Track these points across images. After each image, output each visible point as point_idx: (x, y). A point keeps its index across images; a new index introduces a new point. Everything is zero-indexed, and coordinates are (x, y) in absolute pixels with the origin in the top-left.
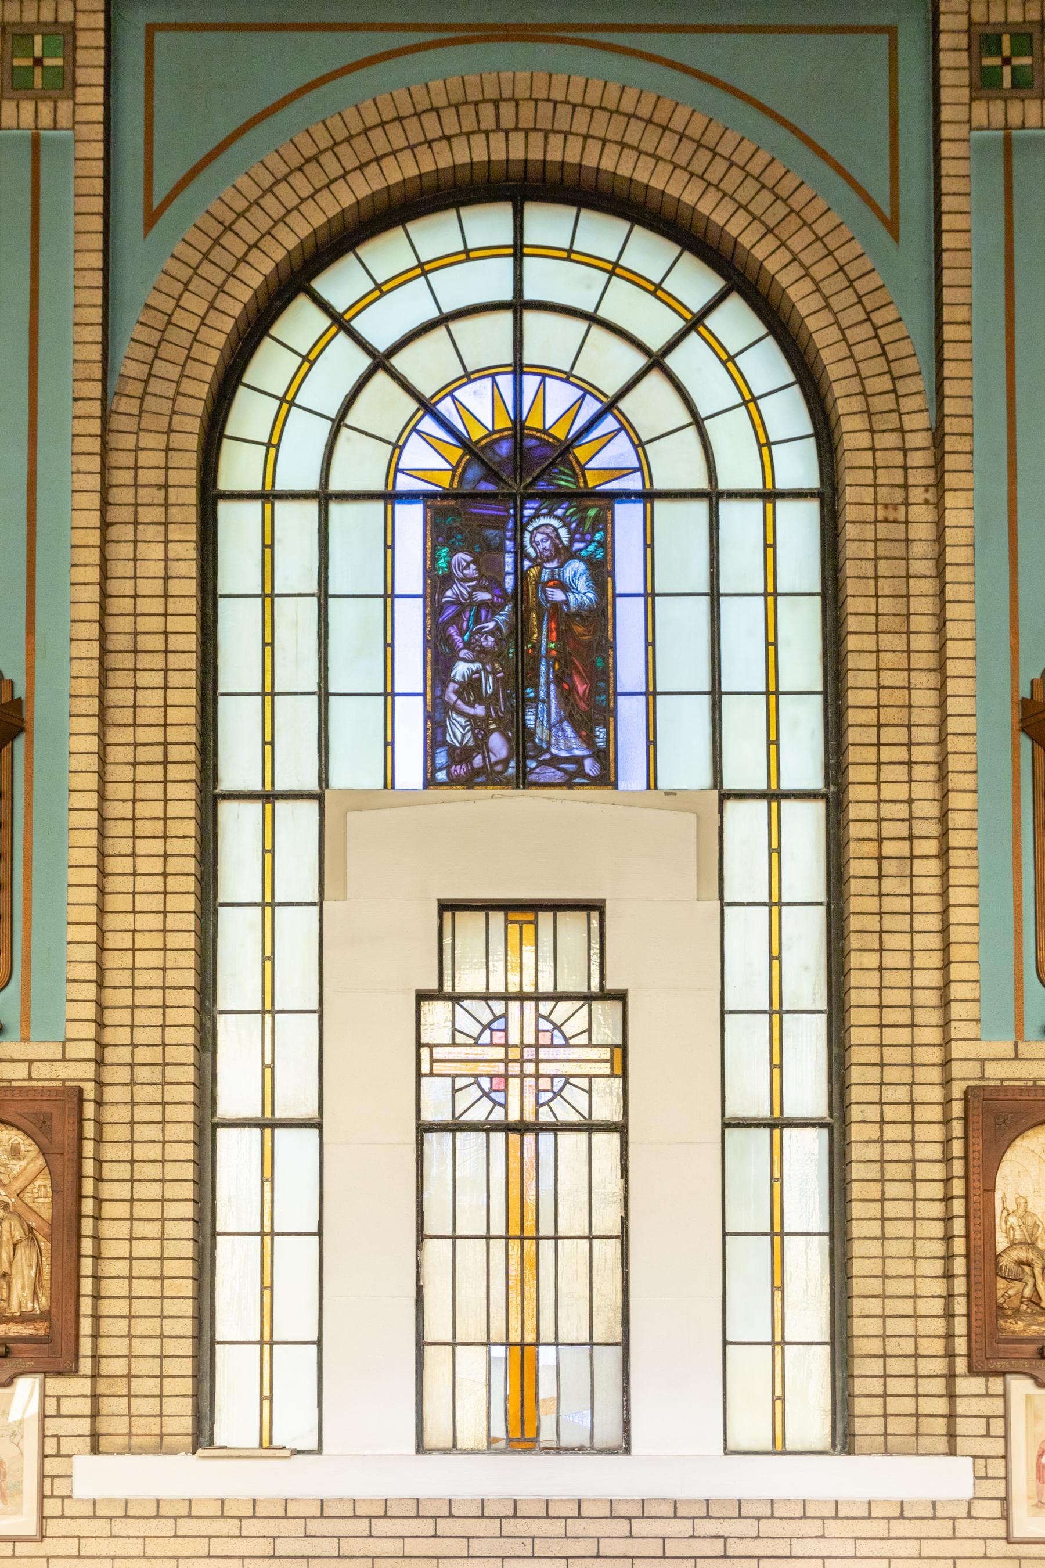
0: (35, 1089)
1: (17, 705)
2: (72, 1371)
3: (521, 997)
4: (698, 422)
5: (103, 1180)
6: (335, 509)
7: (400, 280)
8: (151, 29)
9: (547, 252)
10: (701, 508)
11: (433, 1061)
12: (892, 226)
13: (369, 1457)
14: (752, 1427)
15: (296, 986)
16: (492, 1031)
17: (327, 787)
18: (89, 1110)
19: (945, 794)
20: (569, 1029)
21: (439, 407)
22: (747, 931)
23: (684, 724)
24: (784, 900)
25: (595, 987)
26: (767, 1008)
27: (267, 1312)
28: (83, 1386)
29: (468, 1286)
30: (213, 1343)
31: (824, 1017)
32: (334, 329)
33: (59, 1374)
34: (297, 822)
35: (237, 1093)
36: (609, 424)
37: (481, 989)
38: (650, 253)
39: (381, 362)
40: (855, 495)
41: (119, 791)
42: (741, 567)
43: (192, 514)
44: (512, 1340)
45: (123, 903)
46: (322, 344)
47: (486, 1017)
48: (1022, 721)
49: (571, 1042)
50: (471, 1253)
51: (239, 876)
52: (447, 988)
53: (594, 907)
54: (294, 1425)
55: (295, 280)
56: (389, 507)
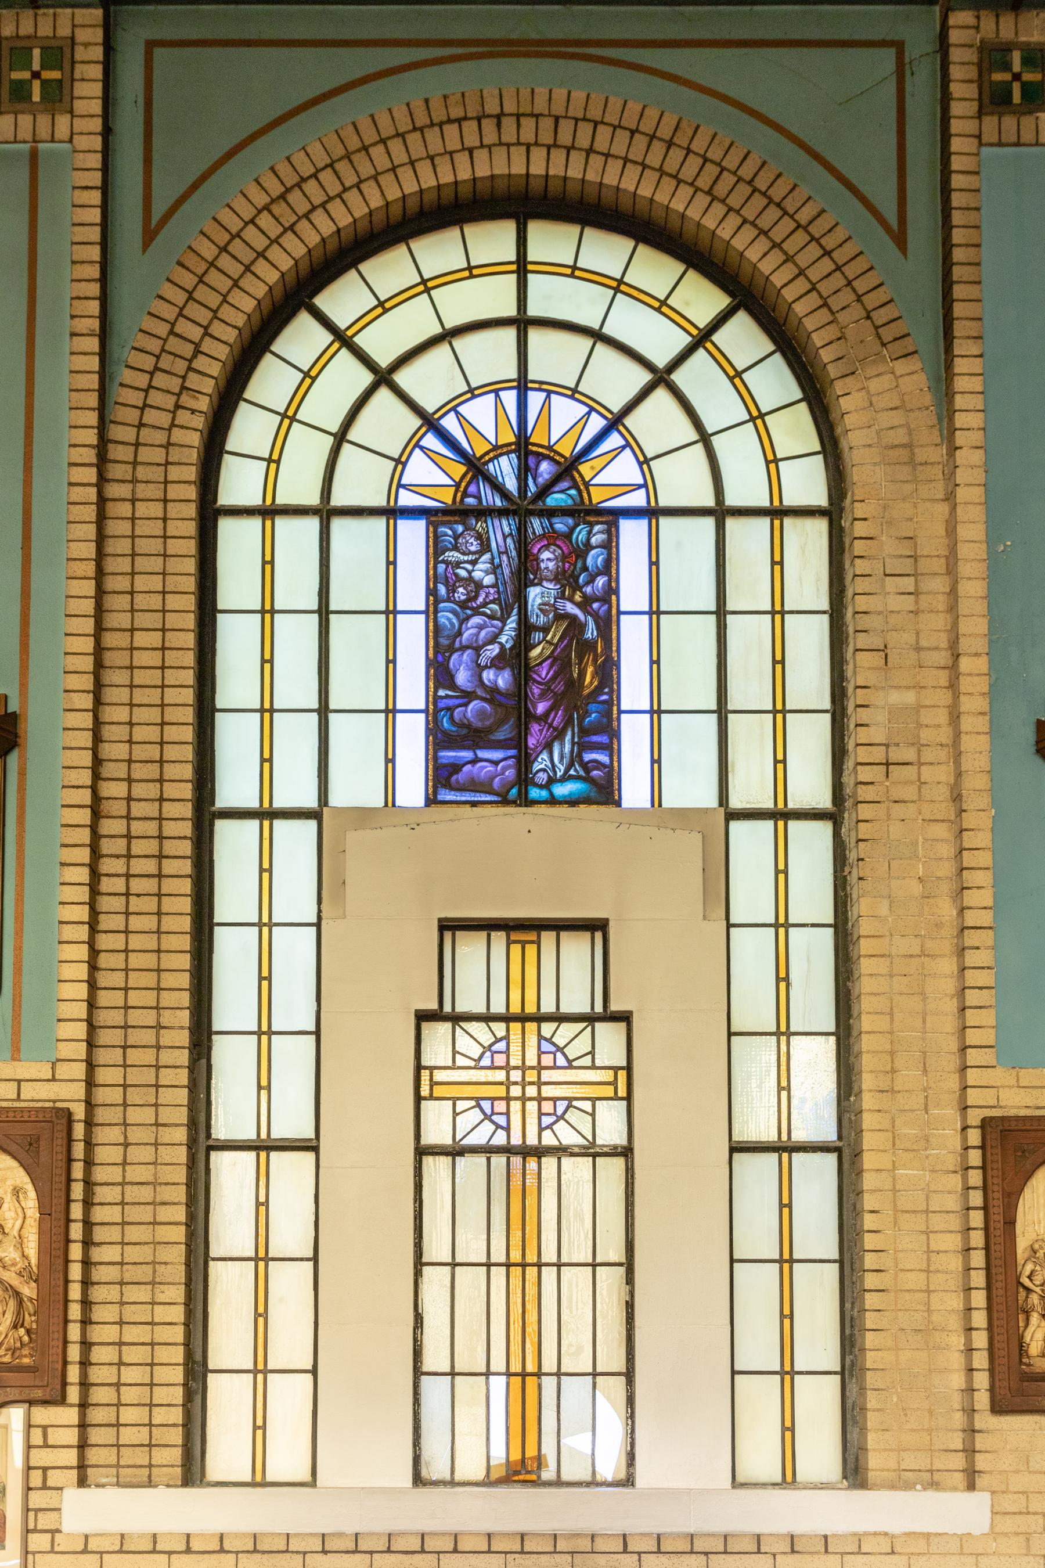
0: (22, 1110)
1: (13, 719)
2: (61, 1400)
3: (523, 1018)
4: (705, 438)
5: (91, 1323)
6: (338, 525)
7: (404, 296)
8: (151, 45)
9: (552, 269)
10: (708, 524)
11: (433, 1084)
12: (900, 239)
13: (365, 1476)
14: (761, 1458)
15: (294, 1007)
16: (493, 1113)
17: (326, 804)
18: (79, 1130)
19: (956, 696)
20: (572, 1052)
21: (442, 422)
22: (753, 951)
23: (691, 744)
24: (786, 608)
25: (599, 1008)
26: (778, 1369)
27: (265, 1003)
28: (70, 1415)
29: (466, 1315)
30: (207, 1258)
31: (828, 716)
32: (336, 345)
33: (46, 1402)
34: (295, 841)
35: (232, 1114)
36: (615, 440)
37: (480, 1008)
38: (654, 271)
39: (384, 378)
40: (863, 511)
41: (117, 602)
42: (750, 588)
43: (191, 528)
44: (513, 1370)
45: (110, 1254)
46: (323, 360)
47: (487, 1039)
48: (1037, 742)
49: (575, 1064)
50: (470, 1280)
51: (234, 896)
52: (447, 1008)
53: (597, 927)
54: (287, 1459)
55: (297, 296)
56: (392, 522)
